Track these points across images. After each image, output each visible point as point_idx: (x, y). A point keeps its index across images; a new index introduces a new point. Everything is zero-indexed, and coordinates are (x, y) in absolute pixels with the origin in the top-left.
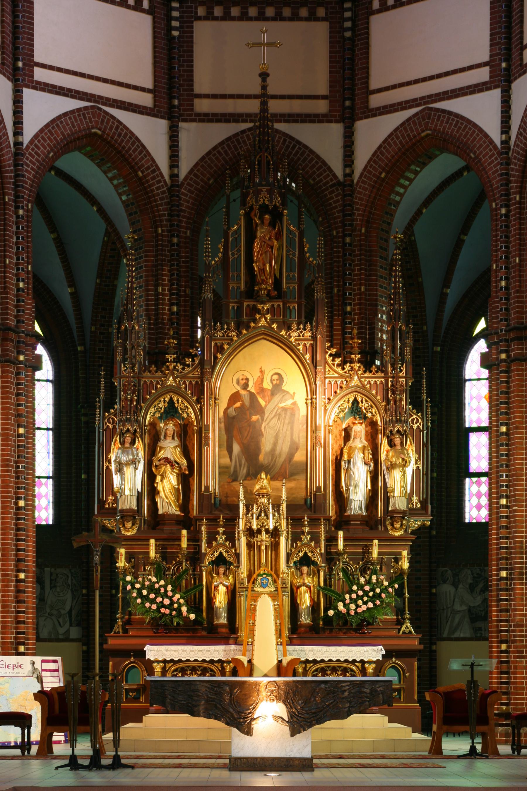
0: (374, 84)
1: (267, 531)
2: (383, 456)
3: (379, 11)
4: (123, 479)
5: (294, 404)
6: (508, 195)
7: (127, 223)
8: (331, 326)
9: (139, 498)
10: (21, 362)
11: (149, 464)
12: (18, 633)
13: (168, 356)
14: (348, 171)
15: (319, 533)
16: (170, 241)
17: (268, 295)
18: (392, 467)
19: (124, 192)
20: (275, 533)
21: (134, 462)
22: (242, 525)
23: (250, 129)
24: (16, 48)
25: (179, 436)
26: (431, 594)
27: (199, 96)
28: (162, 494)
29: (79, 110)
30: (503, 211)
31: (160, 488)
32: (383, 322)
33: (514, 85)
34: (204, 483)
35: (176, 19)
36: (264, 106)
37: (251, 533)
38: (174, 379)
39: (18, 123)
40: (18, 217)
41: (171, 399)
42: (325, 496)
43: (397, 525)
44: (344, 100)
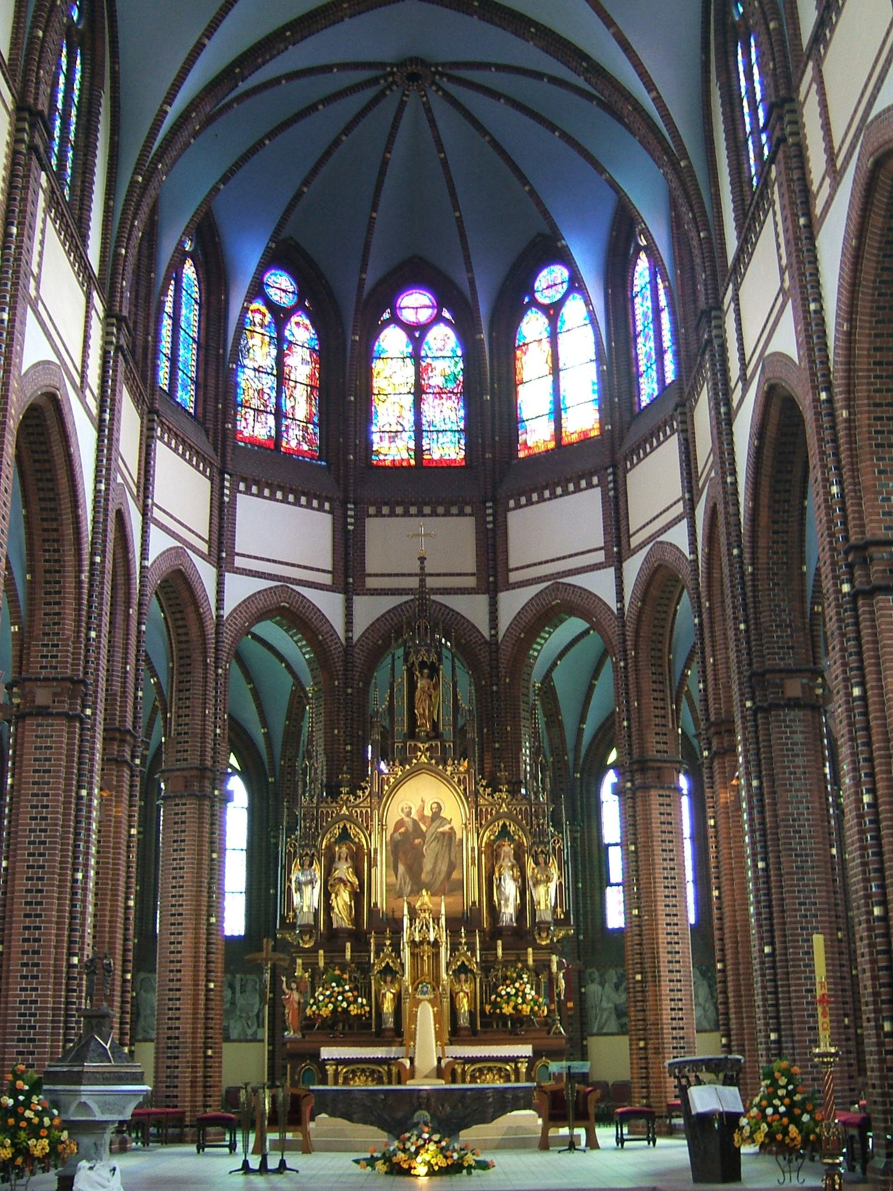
0: (512, 564)
1: (429, 943)
2: (529, 873)
3: (514, 509)
4: (301, 897)
5: (452, 828)
6: (625, 651)
7: (309, 678)
9: (316, 914)
11: (326, 883)
12: (207, 1038)
13: (342, 789)
14: (493, 632)
15: (475, 943)
16: (345, 692)
17: (427, 736)
18: (537, 883)
19: (307, 652)
20: (436, 944)
21: (311, 882)
22: (405, 938)
23: (412, 600)
24: (220, 543)
25: (352, 858)
26: (581, 993)
27: (370, 575)
28: (336, 910)
29: (271, 588)
30: (622, 664)
31: (334, 904)
32: (526, 755)
34: (373, 900)
35: (351, 517)
36: (422, 581)
37: (413, 944)
38: (347, 808)
39: (220, 600)
40: (217, 675)
41: (345, 826)
42: (480, 909)
43: (544, 935)
44: (489, 576)
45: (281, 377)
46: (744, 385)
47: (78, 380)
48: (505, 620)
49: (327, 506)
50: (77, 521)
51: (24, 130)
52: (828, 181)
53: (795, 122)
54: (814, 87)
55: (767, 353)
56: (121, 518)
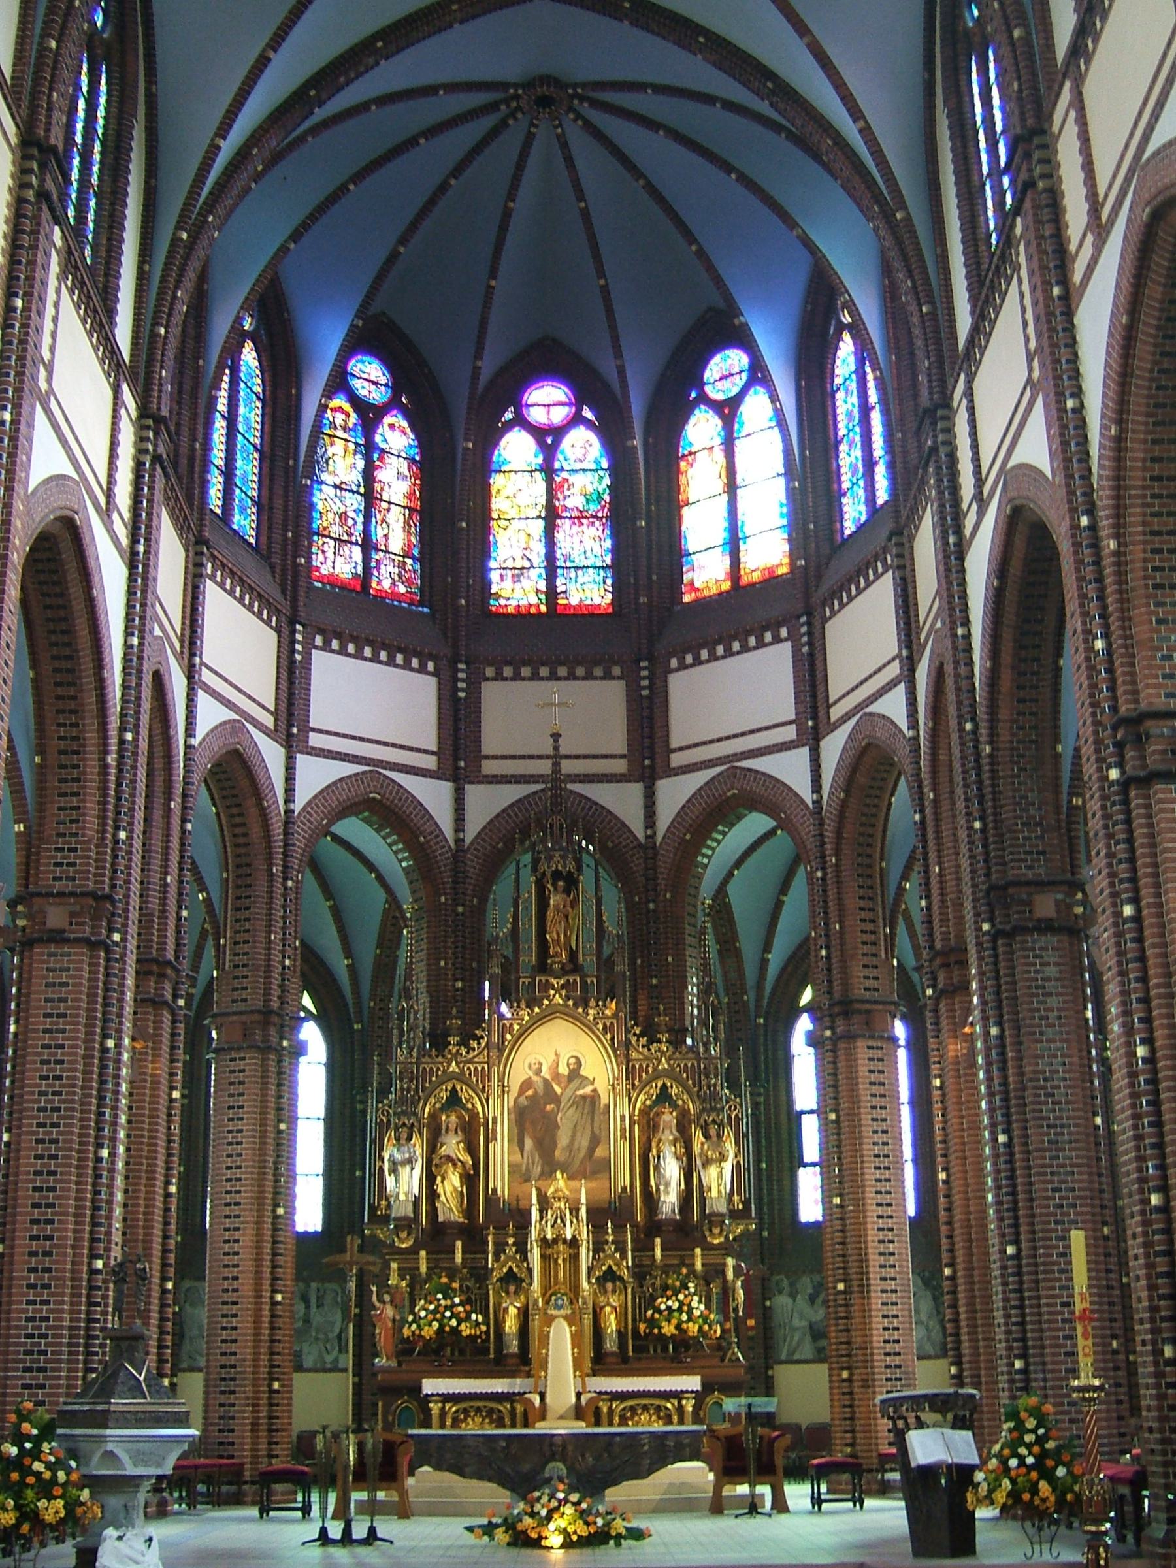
0: (675, 743)
1: (565, 1241)
2: (697, 1149)
3: (677, 670)
4: (397, 1181)
5: (595, 1090)
7: (408, 893)
8: (634, 1001)
9: (416, 1203)
10: (284, 1048)
11: (429, 1162)
12: (272, 1366)
14: (649, 832)
15: (625, 1242)
16: (454, 911)
17: (562, 968)
18: (707, 1163)
19: (405, 859)
20: (574, 1243)
21: (410, 1161)
22: (534, 1235)
23: (542, 790)
24: (290, 715)
25: (464, 1130)
26: (765, 1308)
27: (487, 757)
29: (357, 774)
30: (819, 874)
31: (440, 1190)
32: (692, 994)
33: (822, 743)
34: (491, 1185)
35: (462, 680)
36: (556, 765)
37: (544, 1242)
38: (457, 1064)
39: (290, 790)
40: (286, 888)
41: (454, 1087)
42: (632, 1197)
43: (716, 1231)
44: (644, 758)
45: (371, 497)
46: (979, 507)
47: (102, 500)
48: (665, 816)
49: (431, 666)
50: (101, 686)
51: (31, 171)
52: (1090, 238)
53: (1047, 161)
54: (1072, 114)
55: (1011, 464)
56: (159, 682)
